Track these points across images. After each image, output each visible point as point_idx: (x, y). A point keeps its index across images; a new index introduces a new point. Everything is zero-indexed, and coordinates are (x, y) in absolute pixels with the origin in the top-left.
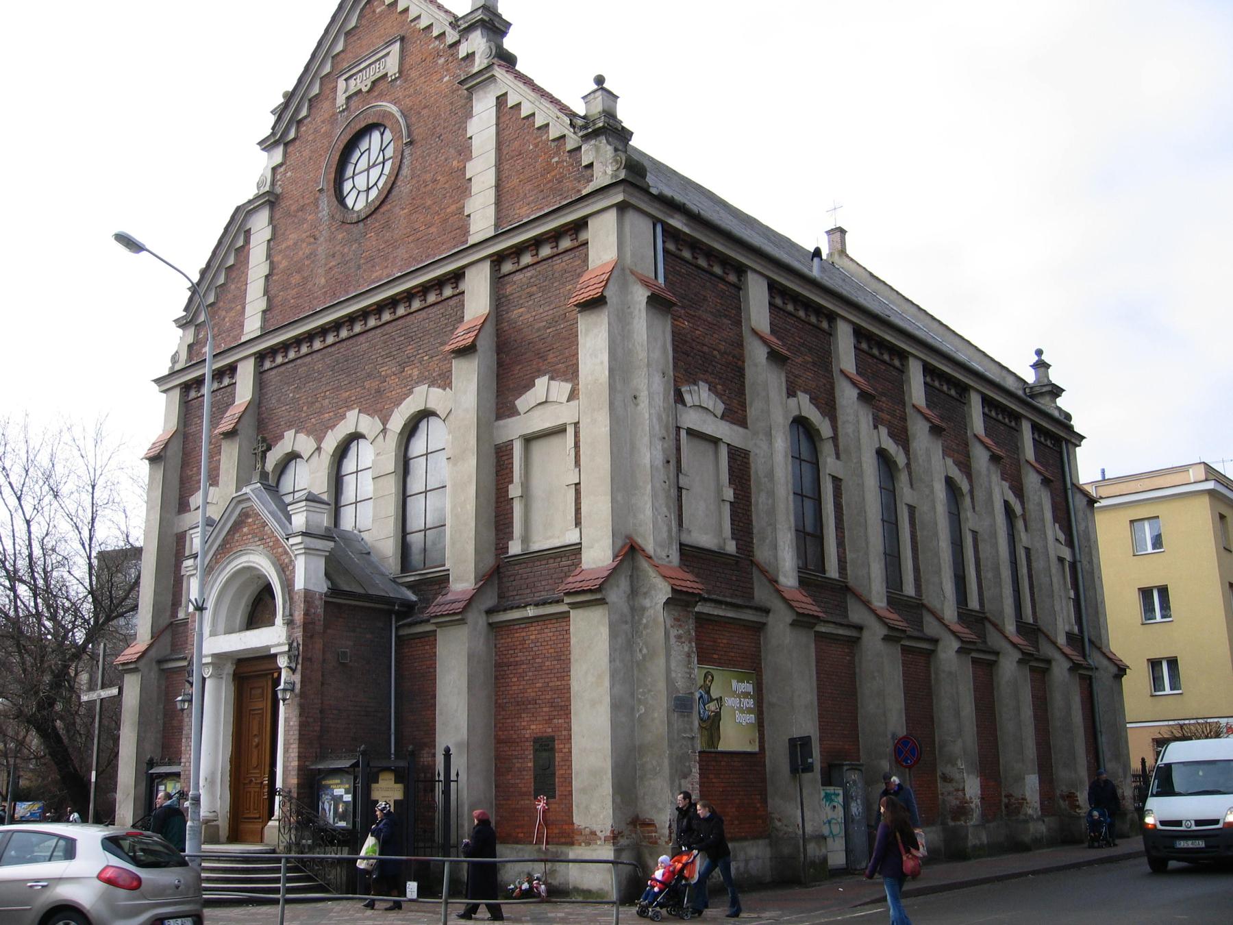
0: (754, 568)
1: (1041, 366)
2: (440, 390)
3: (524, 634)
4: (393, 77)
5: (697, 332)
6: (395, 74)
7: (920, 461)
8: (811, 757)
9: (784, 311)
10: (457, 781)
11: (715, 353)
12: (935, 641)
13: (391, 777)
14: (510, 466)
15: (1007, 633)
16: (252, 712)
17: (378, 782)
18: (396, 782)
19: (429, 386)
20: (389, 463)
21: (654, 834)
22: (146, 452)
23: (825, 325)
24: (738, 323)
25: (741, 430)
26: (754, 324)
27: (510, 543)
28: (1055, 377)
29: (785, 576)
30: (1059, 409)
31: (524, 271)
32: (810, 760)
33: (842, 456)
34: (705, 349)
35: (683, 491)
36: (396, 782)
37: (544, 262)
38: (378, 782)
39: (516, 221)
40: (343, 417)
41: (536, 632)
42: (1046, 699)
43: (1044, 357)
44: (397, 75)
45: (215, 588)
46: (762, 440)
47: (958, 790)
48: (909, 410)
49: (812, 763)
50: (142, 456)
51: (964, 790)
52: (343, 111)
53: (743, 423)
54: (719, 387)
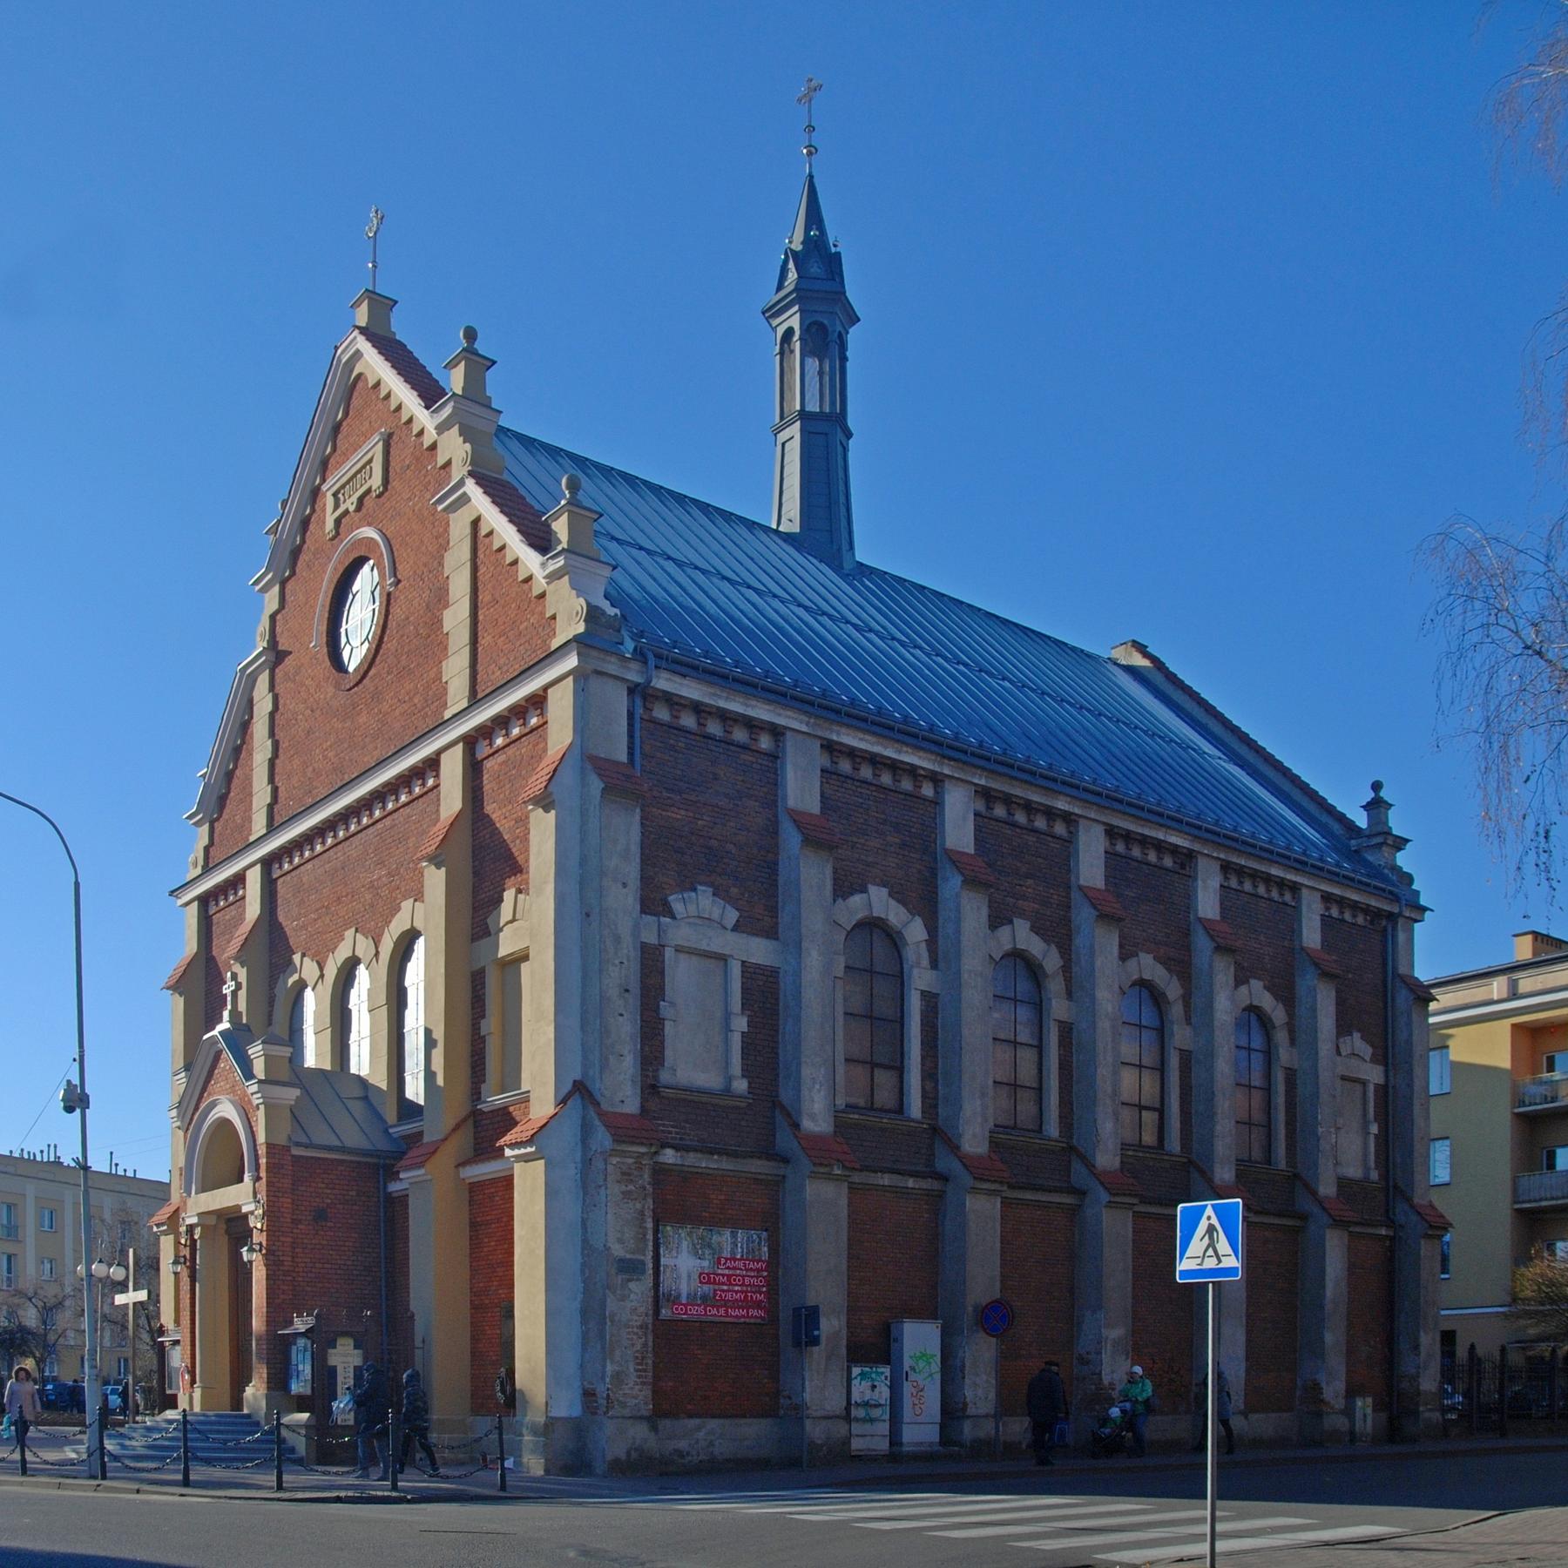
0: (777, 1112)
1: (1376, 806)
3: (493, 1190)
5: (700, 822)
8: (818, 1329)
9: (853, 779)
11: (730, 847)
12: (1081, 1193)
13: (351, 1342)
17: (335, 1347)
19: (415, 900)
22: (166, 980)
23: (927, 790)
25: (773, 942)
28: (1397, 824)
29: (813, 1117)
32: (816, 1333)
33: (941, 965)
34: (714, 843)
35: (666, 1022)
38: (335, 1347)
43: (1382, 794)
45: (630, 1149)
48: (1075, 895)
49: (818, 1336)
50: (163, 985)
51: (1100, 1374)
53: (771, 933)
54: (734, 891)
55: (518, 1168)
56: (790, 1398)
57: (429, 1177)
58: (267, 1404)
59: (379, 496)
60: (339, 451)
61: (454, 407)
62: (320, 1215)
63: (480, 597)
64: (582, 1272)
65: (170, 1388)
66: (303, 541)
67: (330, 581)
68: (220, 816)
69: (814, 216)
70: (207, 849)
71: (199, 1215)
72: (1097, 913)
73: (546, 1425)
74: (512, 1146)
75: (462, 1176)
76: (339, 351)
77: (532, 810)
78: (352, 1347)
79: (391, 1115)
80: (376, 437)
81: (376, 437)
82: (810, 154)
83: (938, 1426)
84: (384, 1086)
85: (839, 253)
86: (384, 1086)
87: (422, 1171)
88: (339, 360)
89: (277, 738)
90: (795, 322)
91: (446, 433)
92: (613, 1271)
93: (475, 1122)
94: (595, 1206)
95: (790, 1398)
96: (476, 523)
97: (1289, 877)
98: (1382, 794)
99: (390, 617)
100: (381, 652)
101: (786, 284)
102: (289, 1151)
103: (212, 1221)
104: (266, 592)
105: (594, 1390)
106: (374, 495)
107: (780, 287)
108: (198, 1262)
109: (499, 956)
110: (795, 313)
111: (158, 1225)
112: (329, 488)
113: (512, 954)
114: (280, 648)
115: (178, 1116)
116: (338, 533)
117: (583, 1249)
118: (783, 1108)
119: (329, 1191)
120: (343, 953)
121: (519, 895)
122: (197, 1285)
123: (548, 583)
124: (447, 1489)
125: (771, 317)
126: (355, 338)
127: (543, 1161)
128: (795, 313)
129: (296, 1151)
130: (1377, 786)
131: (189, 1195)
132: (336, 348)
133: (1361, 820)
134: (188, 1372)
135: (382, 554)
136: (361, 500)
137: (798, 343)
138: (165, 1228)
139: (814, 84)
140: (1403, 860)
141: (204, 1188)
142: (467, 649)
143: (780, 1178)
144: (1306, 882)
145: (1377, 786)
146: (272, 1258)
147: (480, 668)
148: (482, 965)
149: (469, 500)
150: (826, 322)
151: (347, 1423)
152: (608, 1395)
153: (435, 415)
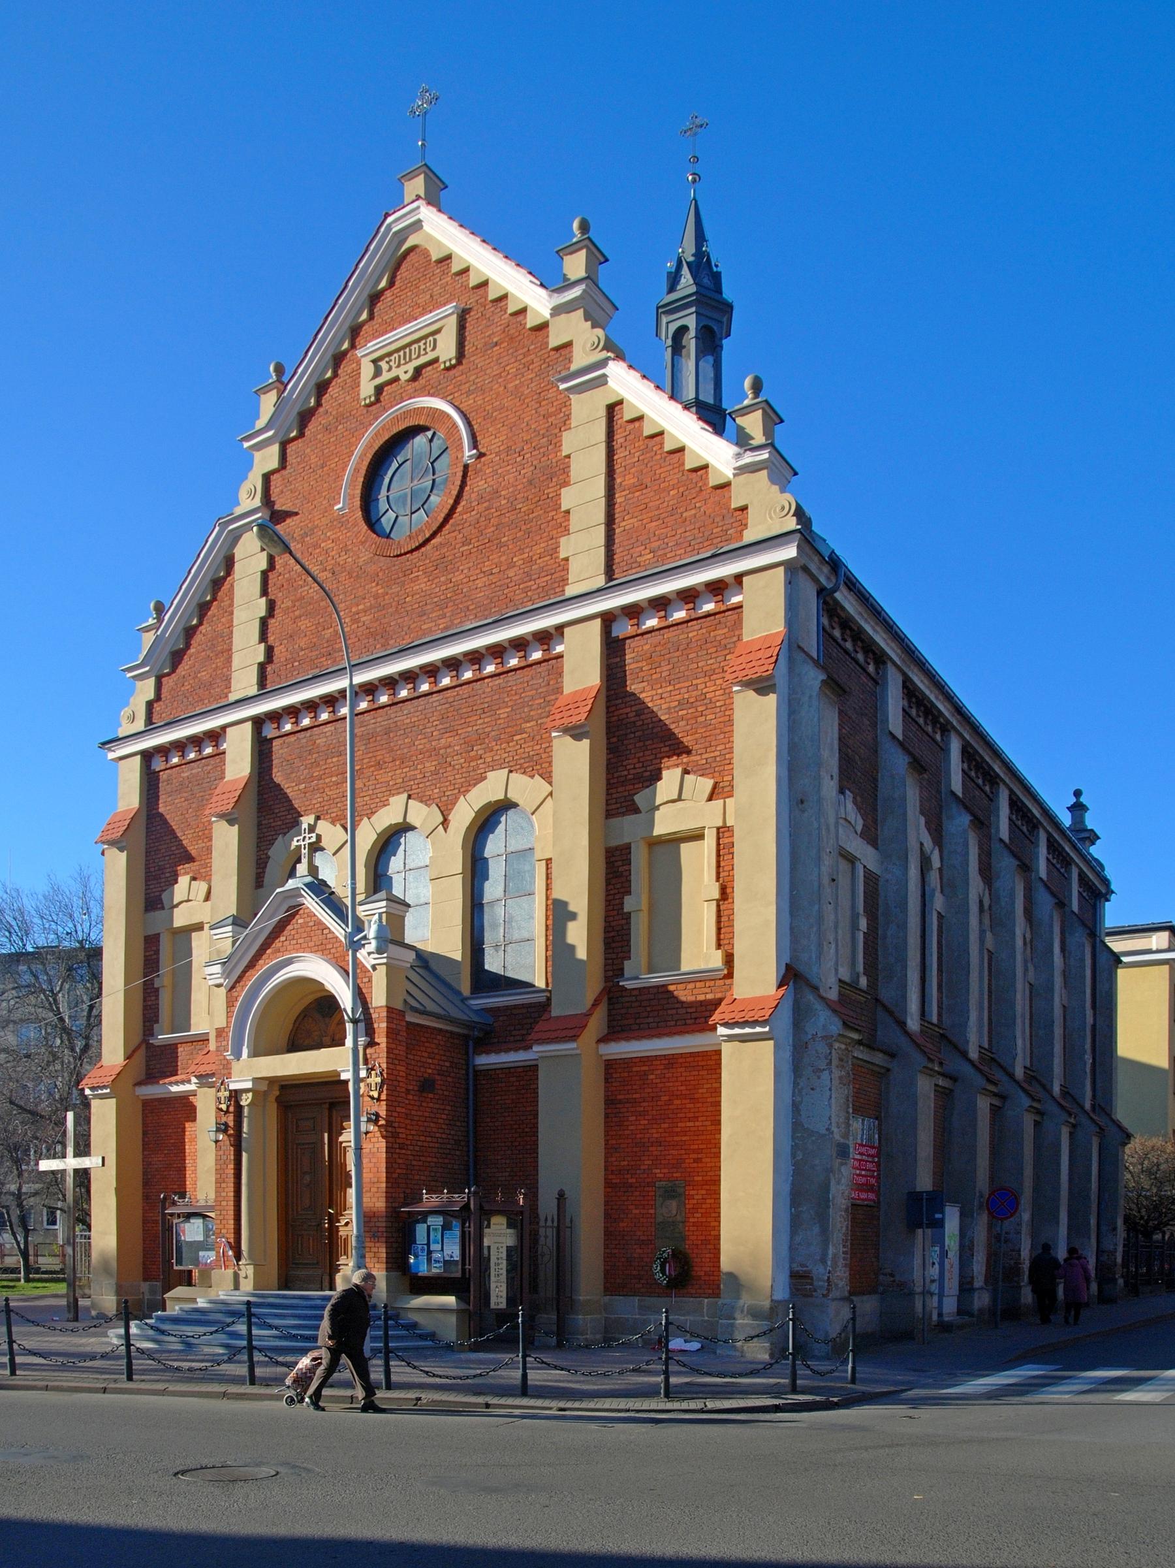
1: (1078, 808)
2: (525, 778)
4: (448, 364)
6: (450, 360)
7: (1003, 904)
10: (571, 1227)
14: (627, 873)
15: (1055, 1094)
16: (873, 1152)
18: (508, 1228)
20: (456, 862)
21: (808, 1287)
24: (874, 725)
26: (891, 728)
27: (626, 962)
28: (1090, 822)
30: (1090, 854)
31: (645, 636)
32: (938, 1216)
36: (508, 1228)
37: (676, 628)
39: (634, 571)
40: (385, 804)
41: (662, 1067)
42: (145, 1145)
44: (453, 362)
46: (894, 864)
47: (1013, 1250)
52: (371, 405)
55: (727, 1049)
56: (892, 1275)
57: (578, 1052)
58: (387, 1285)
59: (447, 369)
60: (377, 320)
61: (584, 291)
62: (426, 1086)
63: (618, 481)
64: (793, 1156)
65: (179, 1262)
66: (319, 404)
67: (369, 446)
68: (173, 671)
69: (700, 237)
70: (150, 705)
71: (255, 1080)
72: (1017, 863)
73: (771, 1308)
74: (726, 1025)
75: (601, 1052)
76: (390, 220)
77: (738, 692)
78: (505, 1226)
79: (465, 988)
80: (449, 308)
81: (449, 308)
82: (694, 181)
83: (956, 1298)
84: (457, 956)
85: (720, 273)
86: (457, 956)
87: (573, 1045)
88: (389, 227)
89: (271, 597)
90: (691, 322)
91: (563, 316)
92: (835, 1155)
93: (609, 999)
94: (812, 1089)
95: (892, 1275)
96: (612, 409)
97: (1071, 854)
98: (1081, 800)
99: (467, 488)
100: (451, 522)
101: (679, 287)
102: (404, 1016)
103: (264, 1087)
104: (258, 450)
105: (810, 1272)
106: (442, 366)
107: (672, 289)
108: (245, 1129)
109: (655, 834)
110: (692, 313)
111: (92, 1089)
112: (369, 349)
113: (669, 834)
114: (277, 507)
115: (222, 974)
116: (378, 401)
117: (794, 1131)
118: (886, 1008)
119: (430, 1061)
120: (388, 816)
121: (686, 776)
122: (245, 1155)
123: (735, 475)
124: (763, 1384)
125: (664, 313)
126: (418, 208)
127: (772, 1042)
128: (692, 313)
129: (411, 1018)
130: (1078, 793)
131: (238, 1055)
132: (387, 215)
133: (1066, 820)
134: (231, 1248)
135: (455, 425)
136: (418, 371)
137: (693, 341)
138: (108, 1091)
139: (698, 121)
140: (1095, 851)
141: (255, 1053)
142: (602, 528)
143: (883, 1071)
144: (1077, 860)
145: (1078, 793)
146: (390, 1129)
147: (617, 548)
148: (627, 840)
149: (606, 383)
150: (715, 328)
151: (499, 1307)
152: (829, 1277)
153: (556, 295)
